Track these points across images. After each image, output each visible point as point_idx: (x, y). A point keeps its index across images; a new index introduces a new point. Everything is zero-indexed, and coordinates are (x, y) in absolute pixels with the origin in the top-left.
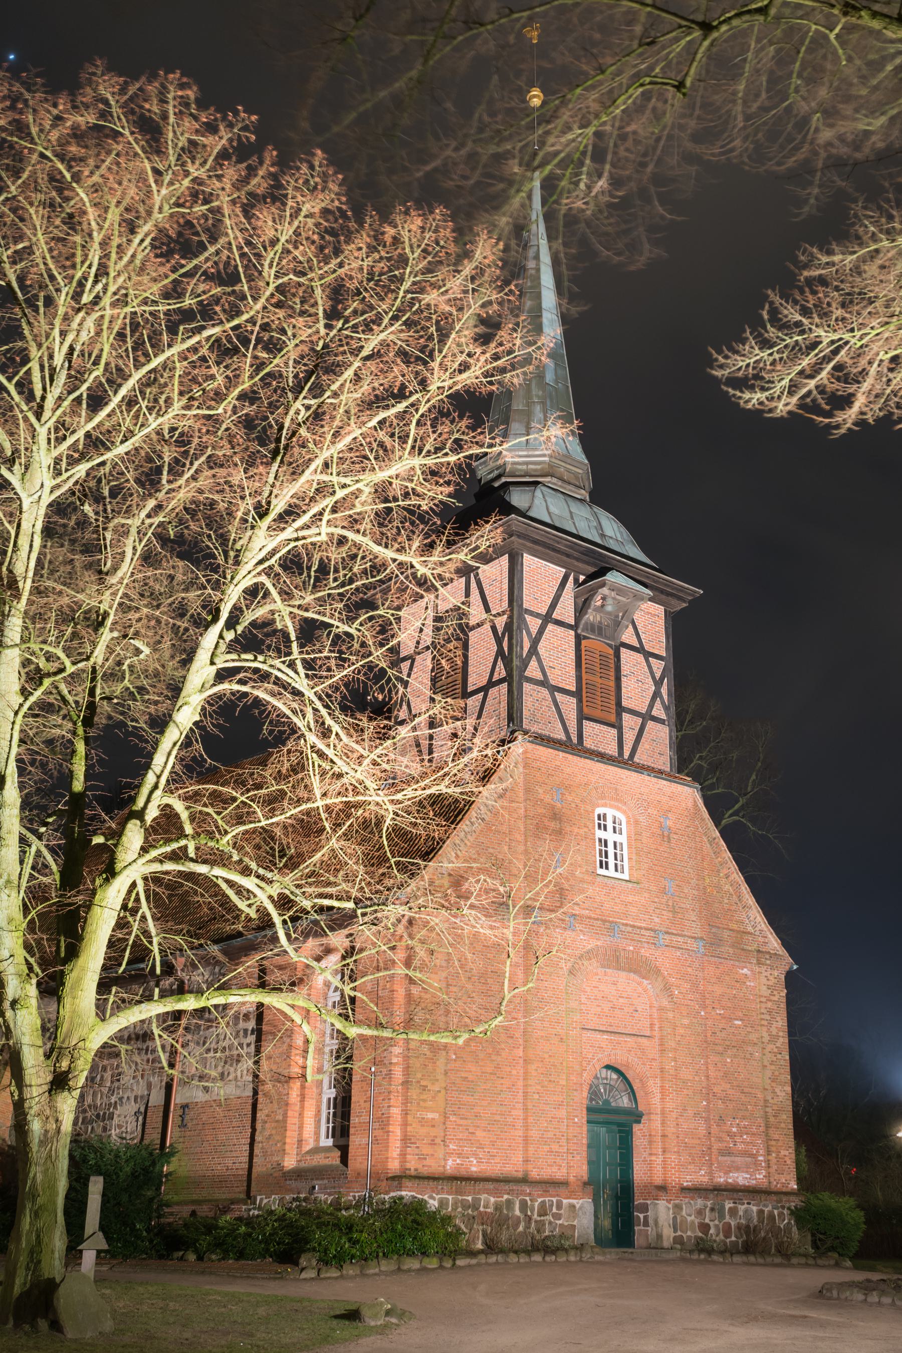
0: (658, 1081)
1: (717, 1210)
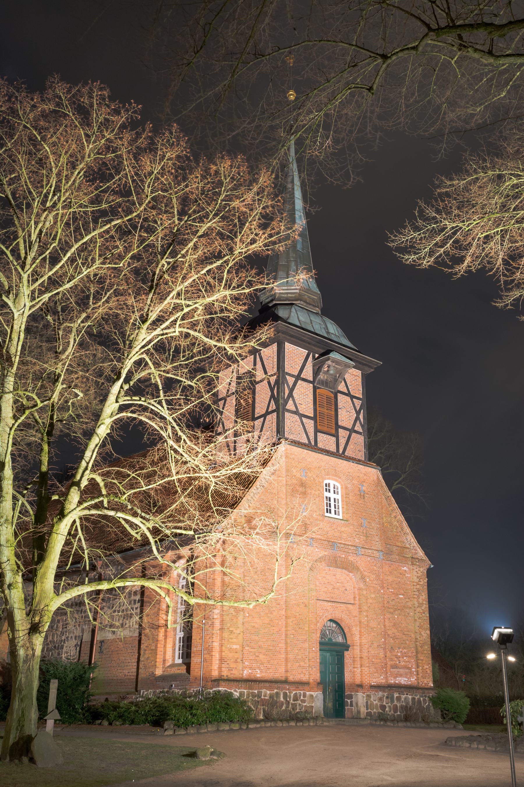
0: (358, 628)
1: (390, 698)
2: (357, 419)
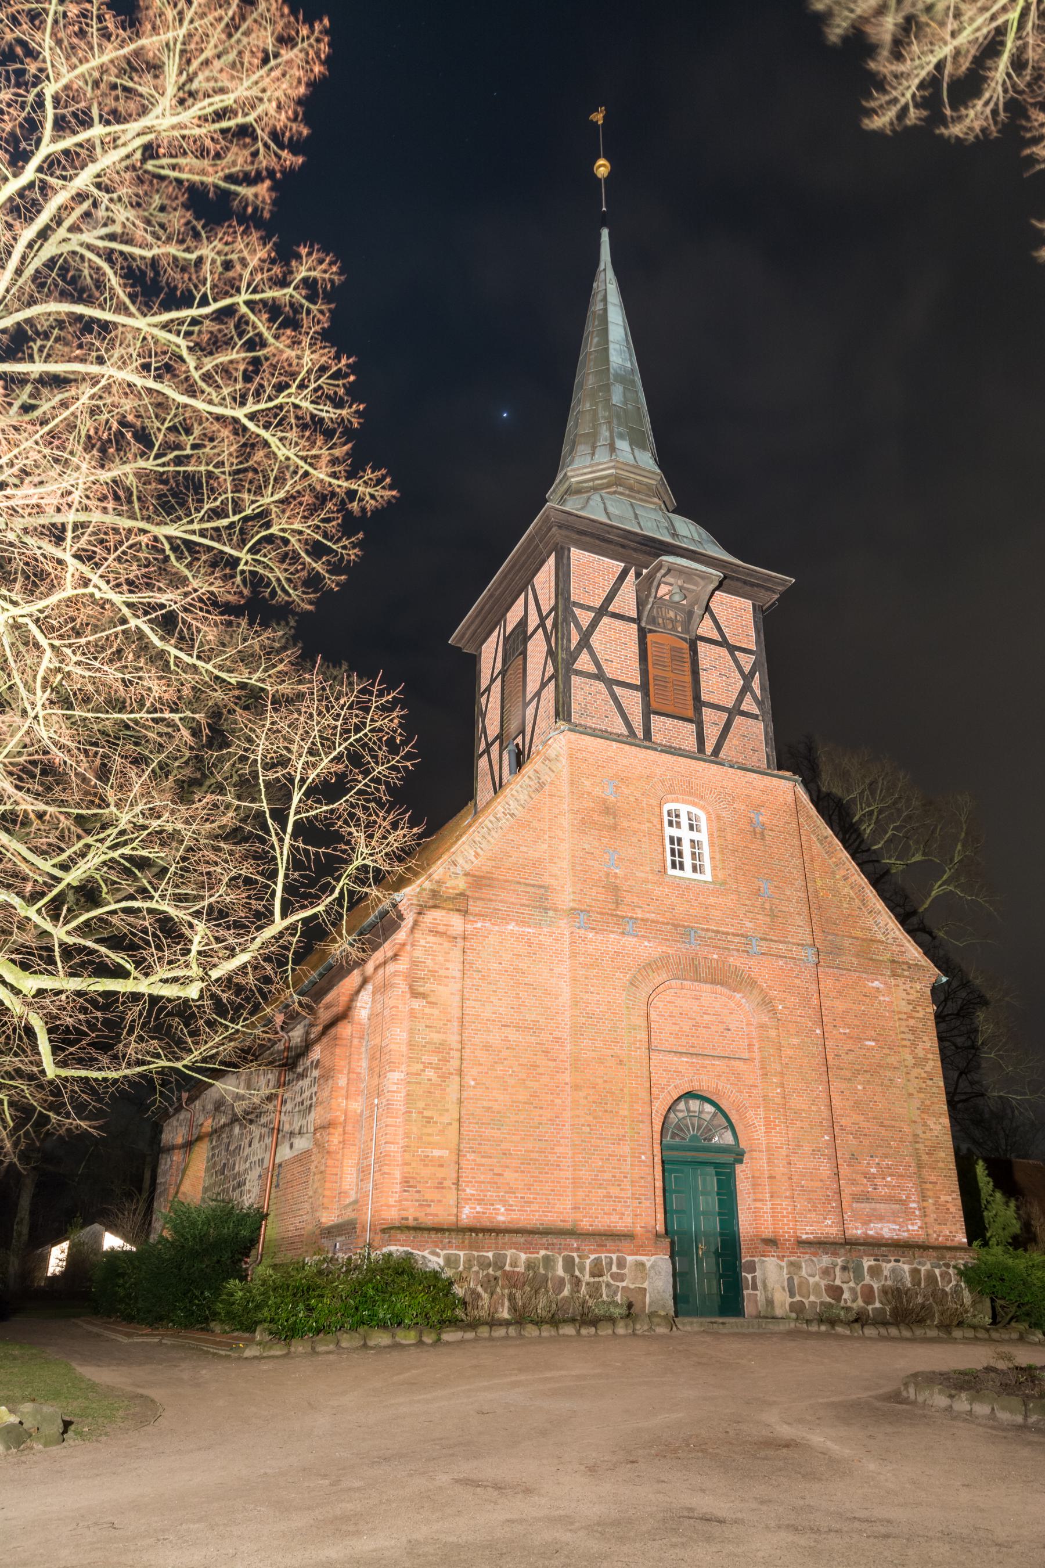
1: (853, 1269)
2: (746, 689)
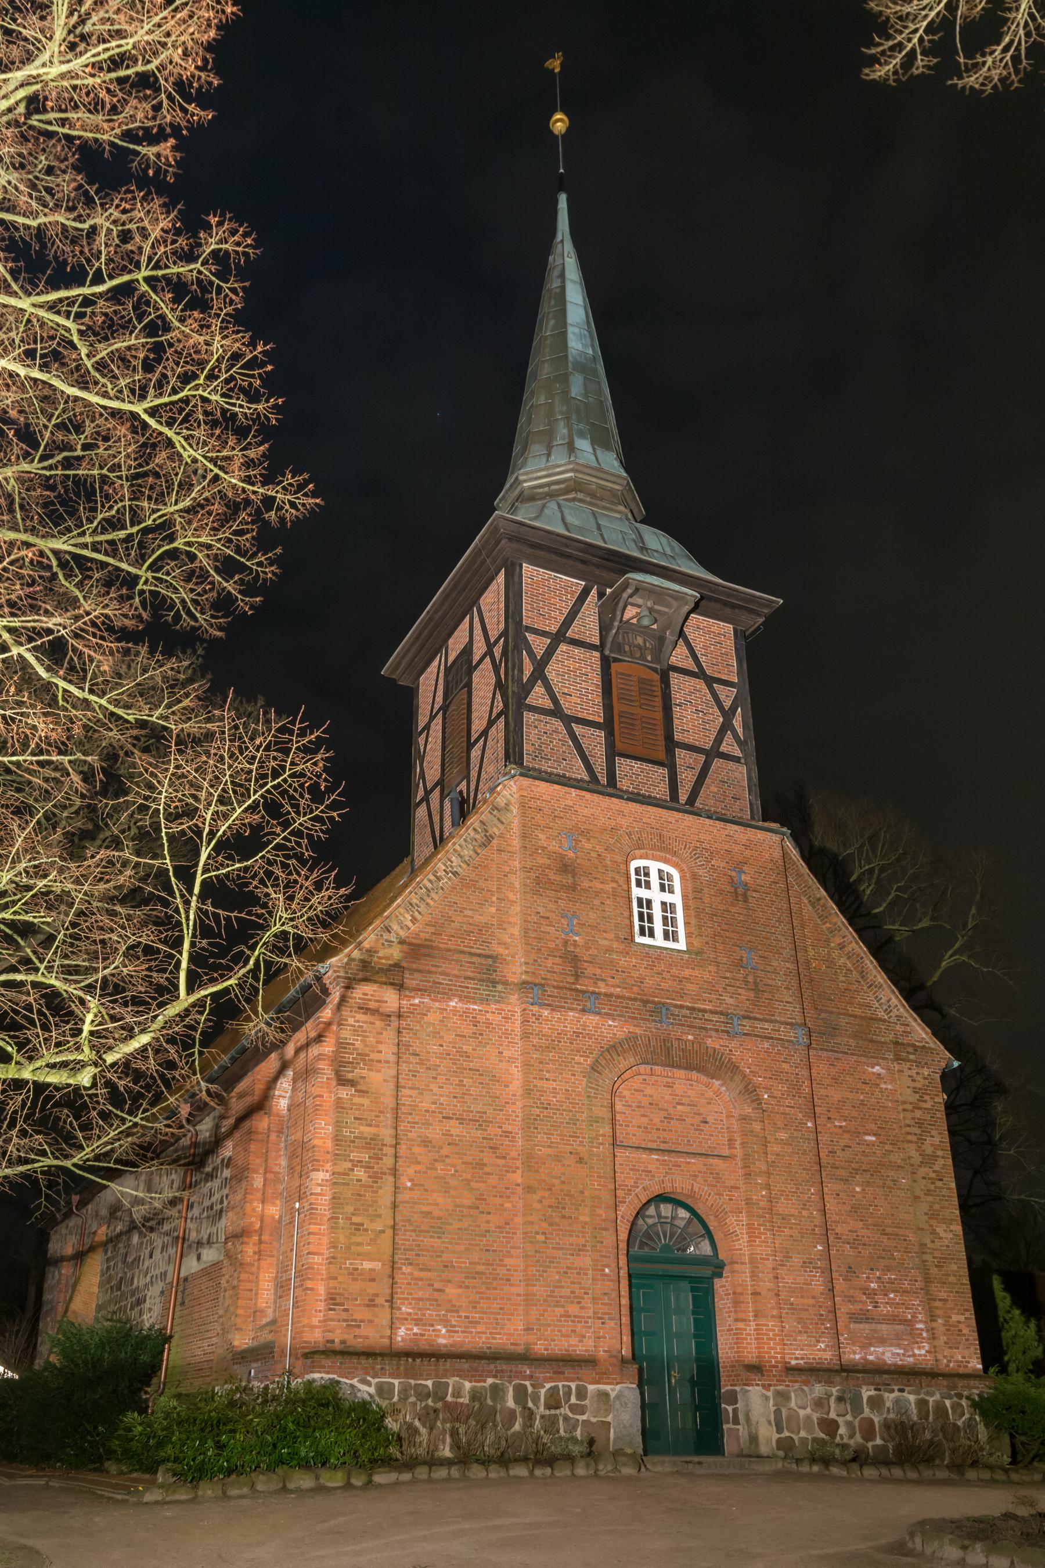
0: (743, 1217)
2: (726, 727)
